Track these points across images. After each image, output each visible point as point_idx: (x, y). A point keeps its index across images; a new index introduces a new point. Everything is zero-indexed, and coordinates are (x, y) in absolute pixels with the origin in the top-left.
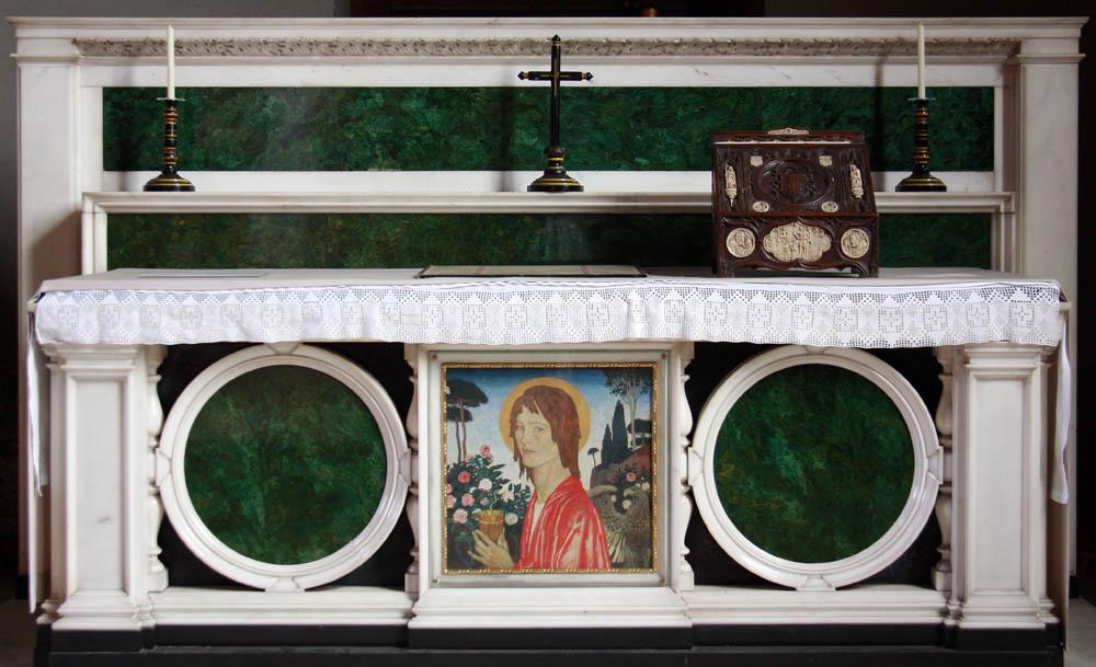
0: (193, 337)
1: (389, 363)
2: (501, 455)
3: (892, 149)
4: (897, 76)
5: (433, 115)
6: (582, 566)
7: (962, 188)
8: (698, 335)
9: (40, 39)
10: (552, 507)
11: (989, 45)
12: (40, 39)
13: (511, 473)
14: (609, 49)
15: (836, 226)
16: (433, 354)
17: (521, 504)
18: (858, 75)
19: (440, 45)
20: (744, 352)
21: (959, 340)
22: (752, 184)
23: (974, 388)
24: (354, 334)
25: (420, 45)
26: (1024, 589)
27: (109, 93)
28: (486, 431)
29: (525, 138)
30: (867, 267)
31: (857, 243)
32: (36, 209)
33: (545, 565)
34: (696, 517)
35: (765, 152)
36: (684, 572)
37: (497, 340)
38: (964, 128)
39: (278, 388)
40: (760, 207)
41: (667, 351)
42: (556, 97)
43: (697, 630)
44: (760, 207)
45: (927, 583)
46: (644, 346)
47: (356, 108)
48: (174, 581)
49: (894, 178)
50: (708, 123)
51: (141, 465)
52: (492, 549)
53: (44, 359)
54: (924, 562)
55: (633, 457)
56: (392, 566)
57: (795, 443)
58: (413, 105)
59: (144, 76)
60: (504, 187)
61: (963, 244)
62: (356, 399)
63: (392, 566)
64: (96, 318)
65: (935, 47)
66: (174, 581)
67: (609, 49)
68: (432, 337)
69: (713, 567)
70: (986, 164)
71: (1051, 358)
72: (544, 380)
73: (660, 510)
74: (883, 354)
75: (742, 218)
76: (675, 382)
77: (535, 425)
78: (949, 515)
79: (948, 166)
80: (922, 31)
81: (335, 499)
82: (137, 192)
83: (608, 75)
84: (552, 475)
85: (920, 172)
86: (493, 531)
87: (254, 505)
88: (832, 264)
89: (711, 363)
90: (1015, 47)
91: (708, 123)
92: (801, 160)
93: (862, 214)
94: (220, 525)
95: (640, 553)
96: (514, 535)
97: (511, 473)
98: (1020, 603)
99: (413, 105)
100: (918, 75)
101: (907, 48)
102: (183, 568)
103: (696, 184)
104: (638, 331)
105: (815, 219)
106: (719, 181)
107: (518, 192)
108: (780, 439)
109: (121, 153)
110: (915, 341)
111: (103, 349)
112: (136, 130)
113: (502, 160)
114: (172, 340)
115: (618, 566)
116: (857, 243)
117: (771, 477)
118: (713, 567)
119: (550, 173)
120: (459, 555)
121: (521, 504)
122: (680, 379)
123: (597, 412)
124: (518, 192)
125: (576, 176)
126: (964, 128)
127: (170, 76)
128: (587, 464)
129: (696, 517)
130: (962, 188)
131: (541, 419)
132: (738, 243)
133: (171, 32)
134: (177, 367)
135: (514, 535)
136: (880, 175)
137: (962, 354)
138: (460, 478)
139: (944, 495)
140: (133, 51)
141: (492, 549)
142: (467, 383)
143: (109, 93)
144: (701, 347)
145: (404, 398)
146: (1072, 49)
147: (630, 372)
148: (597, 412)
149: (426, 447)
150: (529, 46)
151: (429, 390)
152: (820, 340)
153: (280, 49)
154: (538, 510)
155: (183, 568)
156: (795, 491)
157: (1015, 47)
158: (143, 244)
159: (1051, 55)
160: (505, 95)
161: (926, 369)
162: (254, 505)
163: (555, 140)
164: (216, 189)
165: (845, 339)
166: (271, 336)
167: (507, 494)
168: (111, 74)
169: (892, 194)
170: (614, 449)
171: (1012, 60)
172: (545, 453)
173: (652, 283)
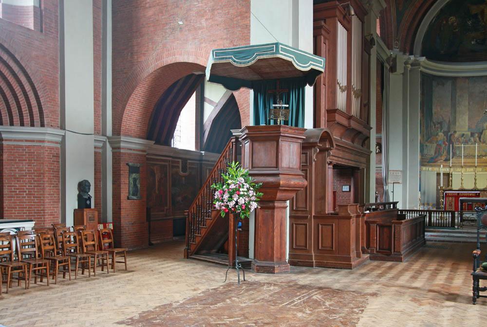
132: (50, 305)
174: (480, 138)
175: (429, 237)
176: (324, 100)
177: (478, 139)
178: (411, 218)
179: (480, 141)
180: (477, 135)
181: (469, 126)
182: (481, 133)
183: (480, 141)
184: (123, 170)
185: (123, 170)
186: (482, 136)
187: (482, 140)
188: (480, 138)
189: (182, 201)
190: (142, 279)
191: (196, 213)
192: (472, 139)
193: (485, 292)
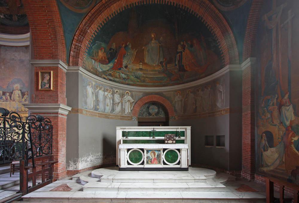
0: (130, 148)
1: (143, 150)
2: (150, 156)
3: (178, 135)
4: (178, 130)
5: (145, 133)
6: (156, 163)
7: (182, 138)
8: (163, 148)
9: (118, 128)
10: (154, 159)
11: (184, 128)
12: (118, 128)
13: (151, 157)
14: (157, 128)
15: (173, 141)
16: (145, 149)
17: (151, 159)
18: (175, 130)
19: (165, 128)
20: (167, 149)
21: (181, 148)
22: (167, 138)
23: (182, 152)
24: (140, 148)
25: (144, 128)
26: (186, 165)
27: (122, 132)
28: (149, 154)
29: (152, 135)
30: (175, 143)
31: (174, 142)
32: (118, 140)
33: (153, 163)
34: (163, 160)
35: (168, 136)
36: (163, 164)
37: (150, 148)
38: (183, 134)
39: (135, 151)
40: (168, 139)
41: (161, 149)
42: (154, 132)
43: (163, 168)
44: (168, 139)
45: (179, 165)
46: (160, 149)
47: (140, 132)
48: (128, 165)
49: (178, 137)
50: (164, 134)
51: (126, 157)
52: (150, 162)
53: (119, 150)
54: (179, 163)
55: (159, 156)
56: (143, 164)
57: (170, 155)
58: (144, 132)
59: (125, 130)
60: (150, 138)
61: (182, 142)
62: (177, 153)
63: (143, 164)
64: (123, 147)
65: (180, 128)
66: (128, 165)
67: (157, 128)
68: (145, 148)
69: (165, 164)
70: (184, 136)
71: (188, 149)
72: (153, 151)
73: (161, 160)
74: (176, 149)
75: (166, 140)
76: (162, 151)
77: (152, 154)
78: (181, 160)
79: (181, 136)
80: (180, 127)
81: (139, 159)
82: (125, 138)
83: (157, 130)
84: (154, 157)
85: (179, 137)
86: (150, 161)
87: (133, 159)
88: (173, 143)
89: (164, 150)
90: (186, 128)
91: (164, 134)
92: (171, 136)
93: (175, 140)
94: (131, 161)
95: (160, 162)
96: (151, 161)
97: (151, 157)
98: (185, 166)
99: (144, 132)
100: (179, 130)
101: (179, 128)
102: (129, 164)
103: (164, 138)
104: (159, 148)
105: (171, 140)
106: (165, 137)
107: (151, 138)
108: (169, 155)
109: (123, 136)
110: (178, 148)
111: (124, 149)
112: (124, 134)
113: (150, 136)
114: (128, 148)
115: (158, 163)
116: (174, 142)
117: (168, 157)
118: (165, 164)
119: (179, 137)
120: (147, 163)
121: (151, 159)
122: (162, 151)
123: (157, 153)
124: (151, 138)
125: (155, 137)
126: (183, 134)
127: (127, 130)
128: (156, 157)
129: (163, 160)
130: (182, 138)
131: (153, 154)
132: (166, 142)
133: (127, 127)
134: (128, 150)
135: (151, 161)
136: (177, 137)
137: (181, 149)
138: (147, 158)
139: (180, 159)
140: (124, 129)
141: (150, 162)
142: (148, 151)
143: (122, 132)
144: (128, 149)
145: (144, 152)
146: (190, 129)
147: (159, 150)
148: (157, 153)
149: (145, 155)
150: (152, 128)
151: (145, 152)
152: (172, 148)
153: (134, 128)
154: (153, 160)
155: (129, 164)
156: (170, 158)
157: (186, 128)
158: (125, 142)
159: (189, 128)
160: (150, 132)
161: (179, 150)
162: (133, 159)
163: (154, 135)
164: (130, 138)
165: (173, 148)
166: (135, 148)
167: (151, 159)
168: (123, 130)
169: (177, 138)
170: (158, 156)
171: (186, 129)
172: (153, 156)
173: (160, 144)
174: (10, 97)
175: (66, 201)
176: (173, 88)
177: (9, 97)
178: (112, 17)
179: (11, 99)
180: (8, 94)
181: (58, 86)
182: (12, 93)
183: (11, 99)
184: (250, 145)
185: (250, 145)
186: (12, 95)
187: (12, 98)
188: (10, 97)
189: (90, 85)
190: (130, 116)
191: (41, 52)
192: (4, 97)
193: (163, 1)
